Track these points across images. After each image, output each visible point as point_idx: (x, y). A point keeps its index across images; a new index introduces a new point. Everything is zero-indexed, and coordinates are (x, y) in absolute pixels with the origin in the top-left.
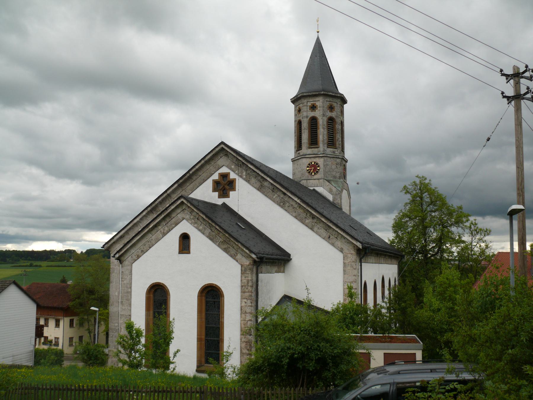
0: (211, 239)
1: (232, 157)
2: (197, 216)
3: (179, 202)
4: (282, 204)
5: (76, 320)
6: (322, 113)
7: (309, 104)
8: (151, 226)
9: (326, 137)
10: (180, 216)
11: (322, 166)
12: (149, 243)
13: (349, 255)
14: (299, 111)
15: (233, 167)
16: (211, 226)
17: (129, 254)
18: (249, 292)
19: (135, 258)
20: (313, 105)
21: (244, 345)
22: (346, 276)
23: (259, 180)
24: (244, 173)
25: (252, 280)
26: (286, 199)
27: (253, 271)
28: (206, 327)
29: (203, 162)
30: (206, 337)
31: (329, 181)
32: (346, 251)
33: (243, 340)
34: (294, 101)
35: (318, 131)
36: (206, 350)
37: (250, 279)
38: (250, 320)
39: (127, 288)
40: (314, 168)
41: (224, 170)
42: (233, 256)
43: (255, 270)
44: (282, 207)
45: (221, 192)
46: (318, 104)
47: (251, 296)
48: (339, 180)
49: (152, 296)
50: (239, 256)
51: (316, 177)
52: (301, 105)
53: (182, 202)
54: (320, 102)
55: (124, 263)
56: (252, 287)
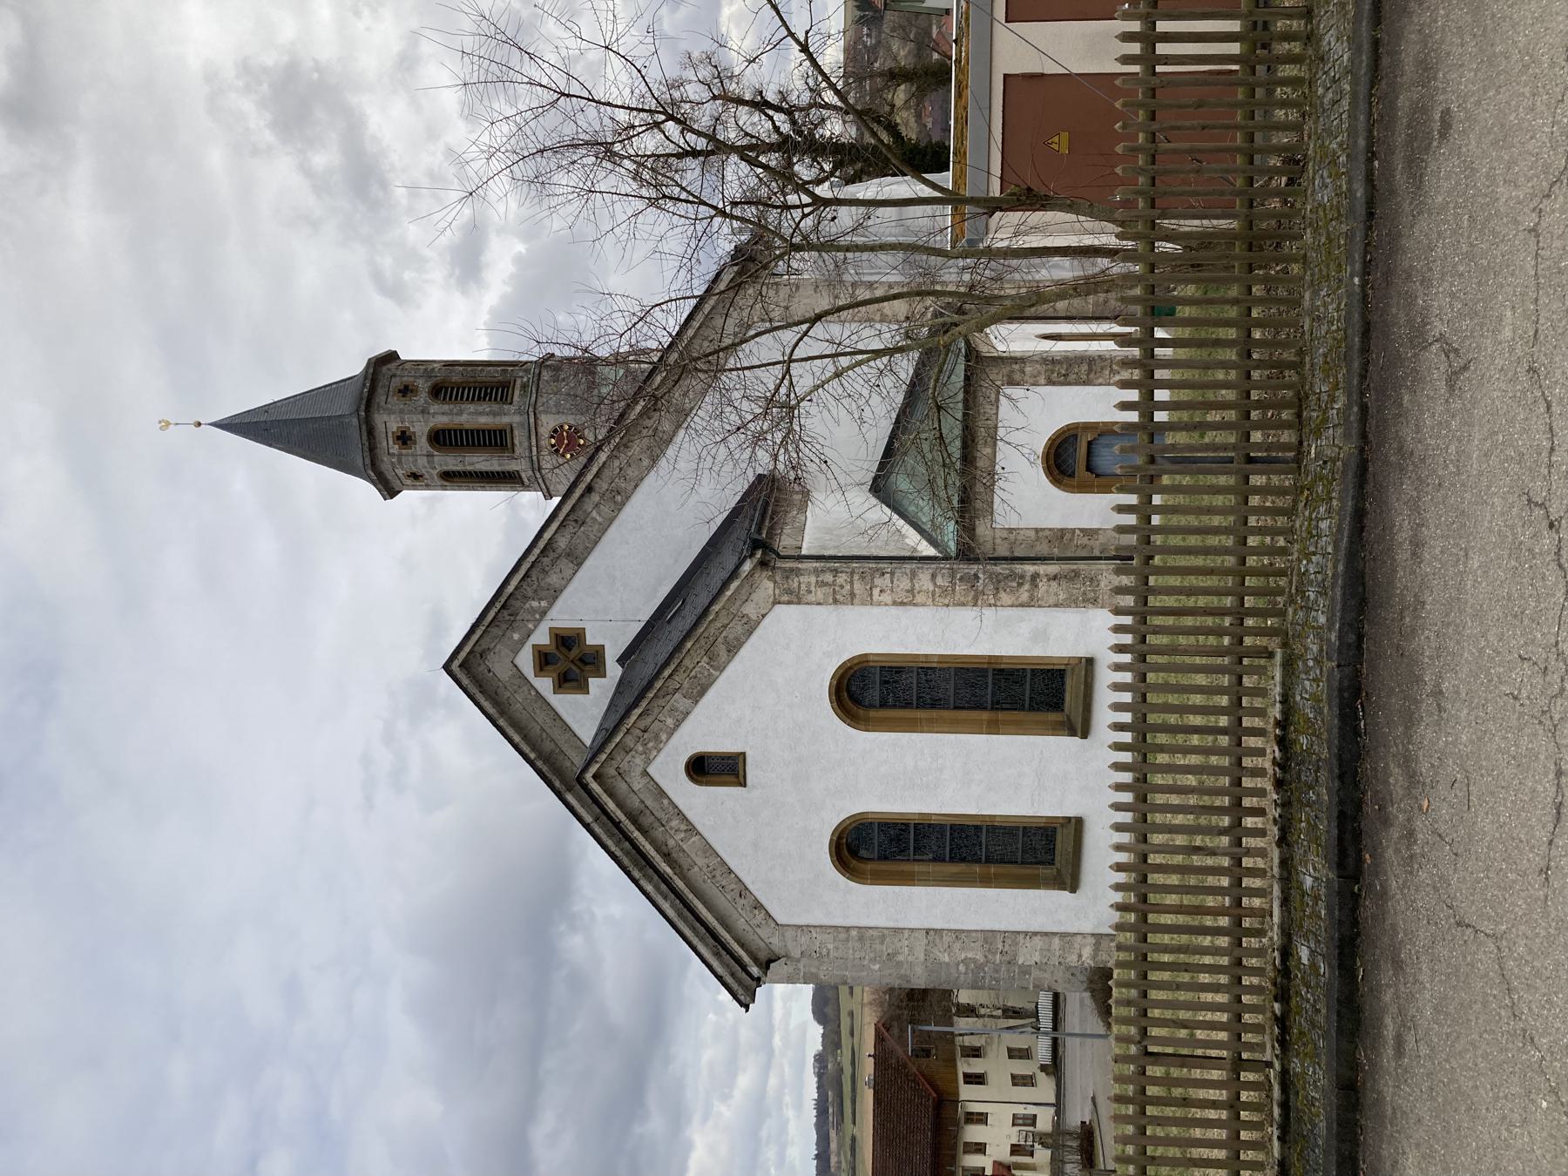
0: (703, 692)
1: (487, 638)
4: (619, 498)
5: (965, 1066)
7: (395, 449)
8: (668, 870)
9: (485, 407)
10: (638, 784)
11: (561, 419)
12: (718, 873)
14: (415, 476)
15: (516, 636)
16: (665, 693)
17: (750, 937)
18: (852, 583)
19: (760, 916)
20: (398, 438)
21: (1005, 598)
24: (535, 604)
25: (817, 572)
26: (603, 485)
27: (792, 570)
28: (956, 708)
29: (501, 722)
30: (985, 708)
34: (389, 491)
35: (467, 426)
36: (1022, 709)
37: (813, 579)
39: (847, 940)
41: (526, 661)
42: (751, 627)
43: (789, 564)
44: (628, 498)
45: (588, 668)
46: (394, 426)
47: (862, 577)
50: (750, 610)
52: (400, 472)
54: (388, 422)
55: (777, 950)
56: (836, 572)
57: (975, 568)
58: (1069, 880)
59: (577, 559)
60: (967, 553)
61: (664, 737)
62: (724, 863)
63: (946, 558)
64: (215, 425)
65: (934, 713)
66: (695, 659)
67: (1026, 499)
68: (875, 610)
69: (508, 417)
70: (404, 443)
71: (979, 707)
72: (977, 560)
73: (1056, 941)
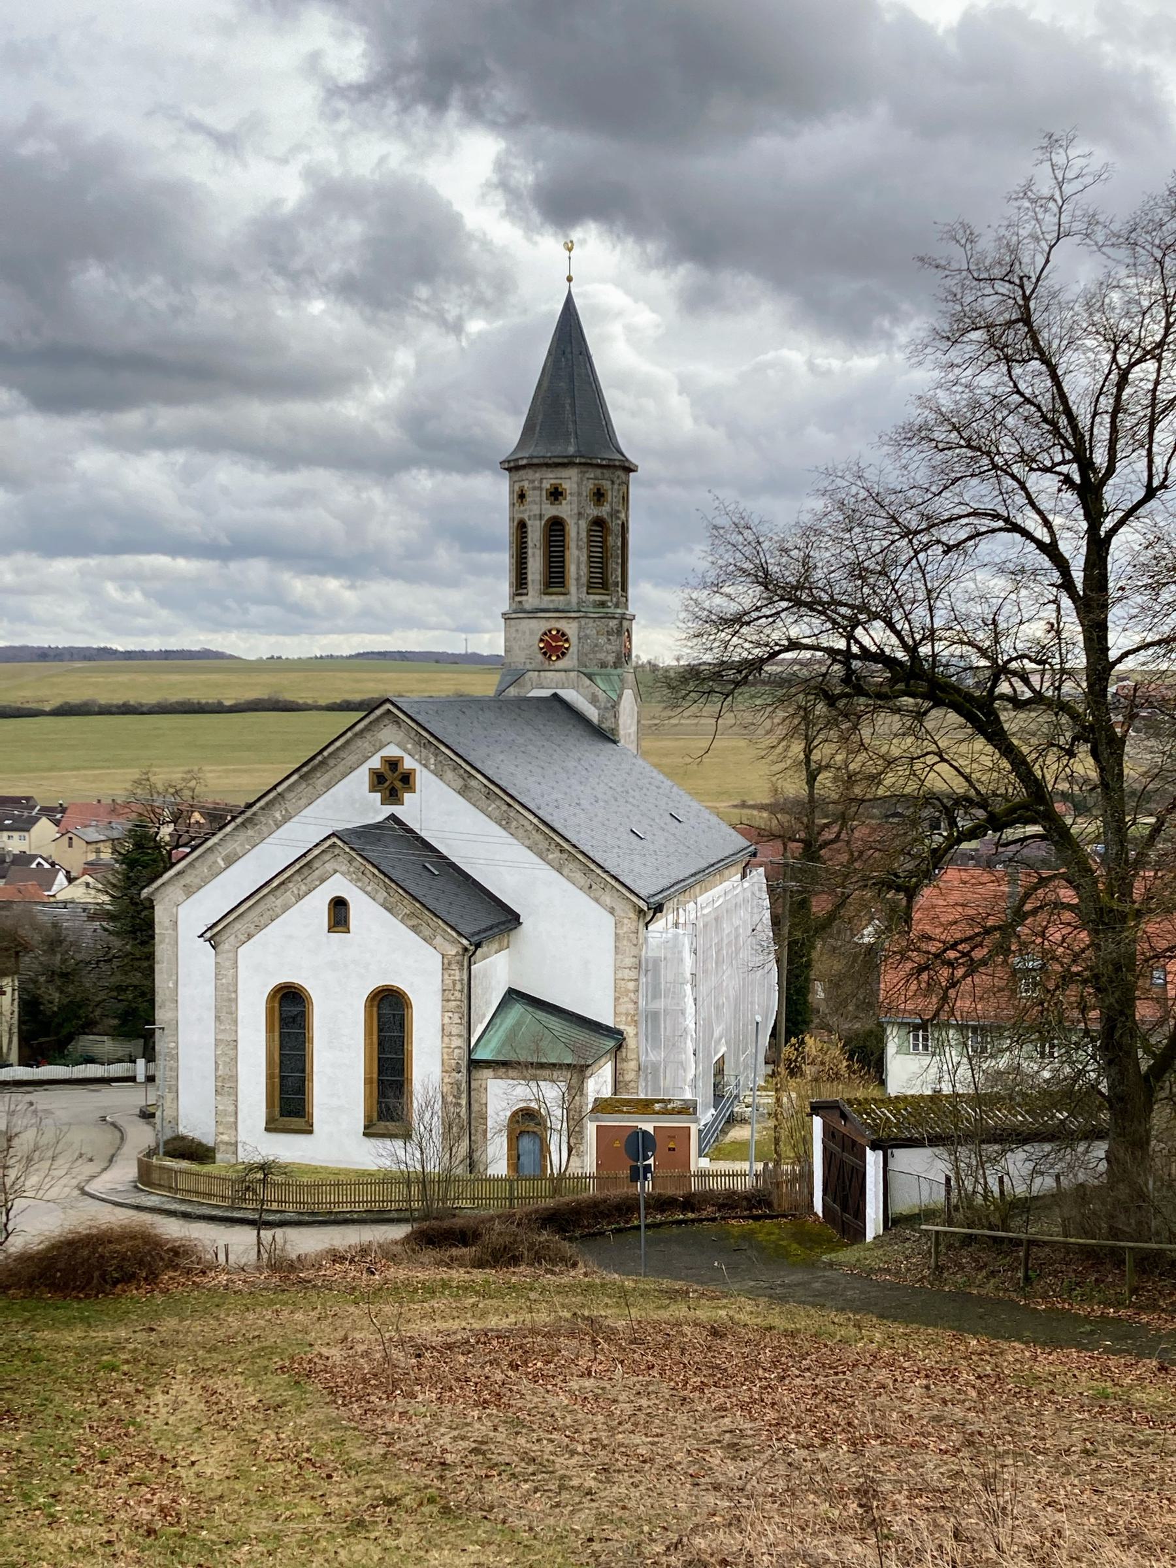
2: (362, 868)
3: (329, 842)
4: (504, 822)
6: (576, 511)
7: (546, 485)
8: (274, 885)
9: (584, 570)
10: (329, 867)
11: (574, 640)
12: (271, 912)
13: (626, 921)
14: (522, 496)
15: (409, 746)
17: (229, 931)
19: (243, 938)
20: (556, 489)
22: (620, 956)
23: (460, 776)
24: (432, 761)
28: (379, 1059)
31: (590, 677)
32: (618, 912)
33: (446, 1080)
35: (567, 553)
38: (459, 1048)
39: (228, 991)
40: (553, 646)
41: (392, 751)
45: (388, 793)
48: (614, 672)
49: (277, 1005)
50: (439, 940)
51: (561, 664)
53: (334, 845)
54: (570, 480)
56: (461, 991)
57: (464, 1070)
58: (272, 1126)
59: (464, 791)
60: (474, 1065)
61: (359, 884)
62: (278, 916)
63: (470, 1053)
64: (569, 303)
65: (376, 1046)
66: (408, 906)
67: (502, 1097)
68: (439, 1013)
69: (575, 592)
70: (552, 494)
71: (380, 1073)
72: (469, 1072)
73: (232, 1119)
